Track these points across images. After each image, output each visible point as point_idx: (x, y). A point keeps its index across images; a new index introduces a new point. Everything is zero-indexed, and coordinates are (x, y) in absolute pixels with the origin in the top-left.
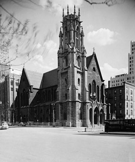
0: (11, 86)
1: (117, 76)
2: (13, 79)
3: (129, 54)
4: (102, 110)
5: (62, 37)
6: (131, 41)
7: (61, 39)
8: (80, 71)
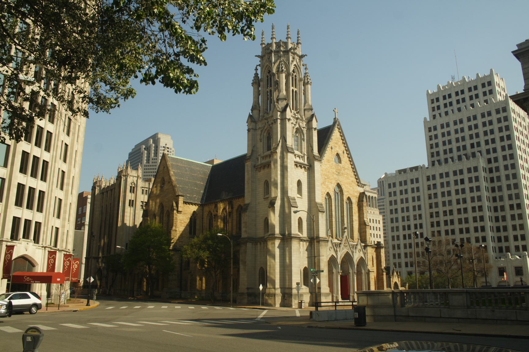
0: (130, 196)
1: (400, 172)
2: (135, 179)
3: (425, 119)
4: (362, 261)
5: (259, 86)
6: (428, 91)
7: (256, 90)
8: (301, 161)
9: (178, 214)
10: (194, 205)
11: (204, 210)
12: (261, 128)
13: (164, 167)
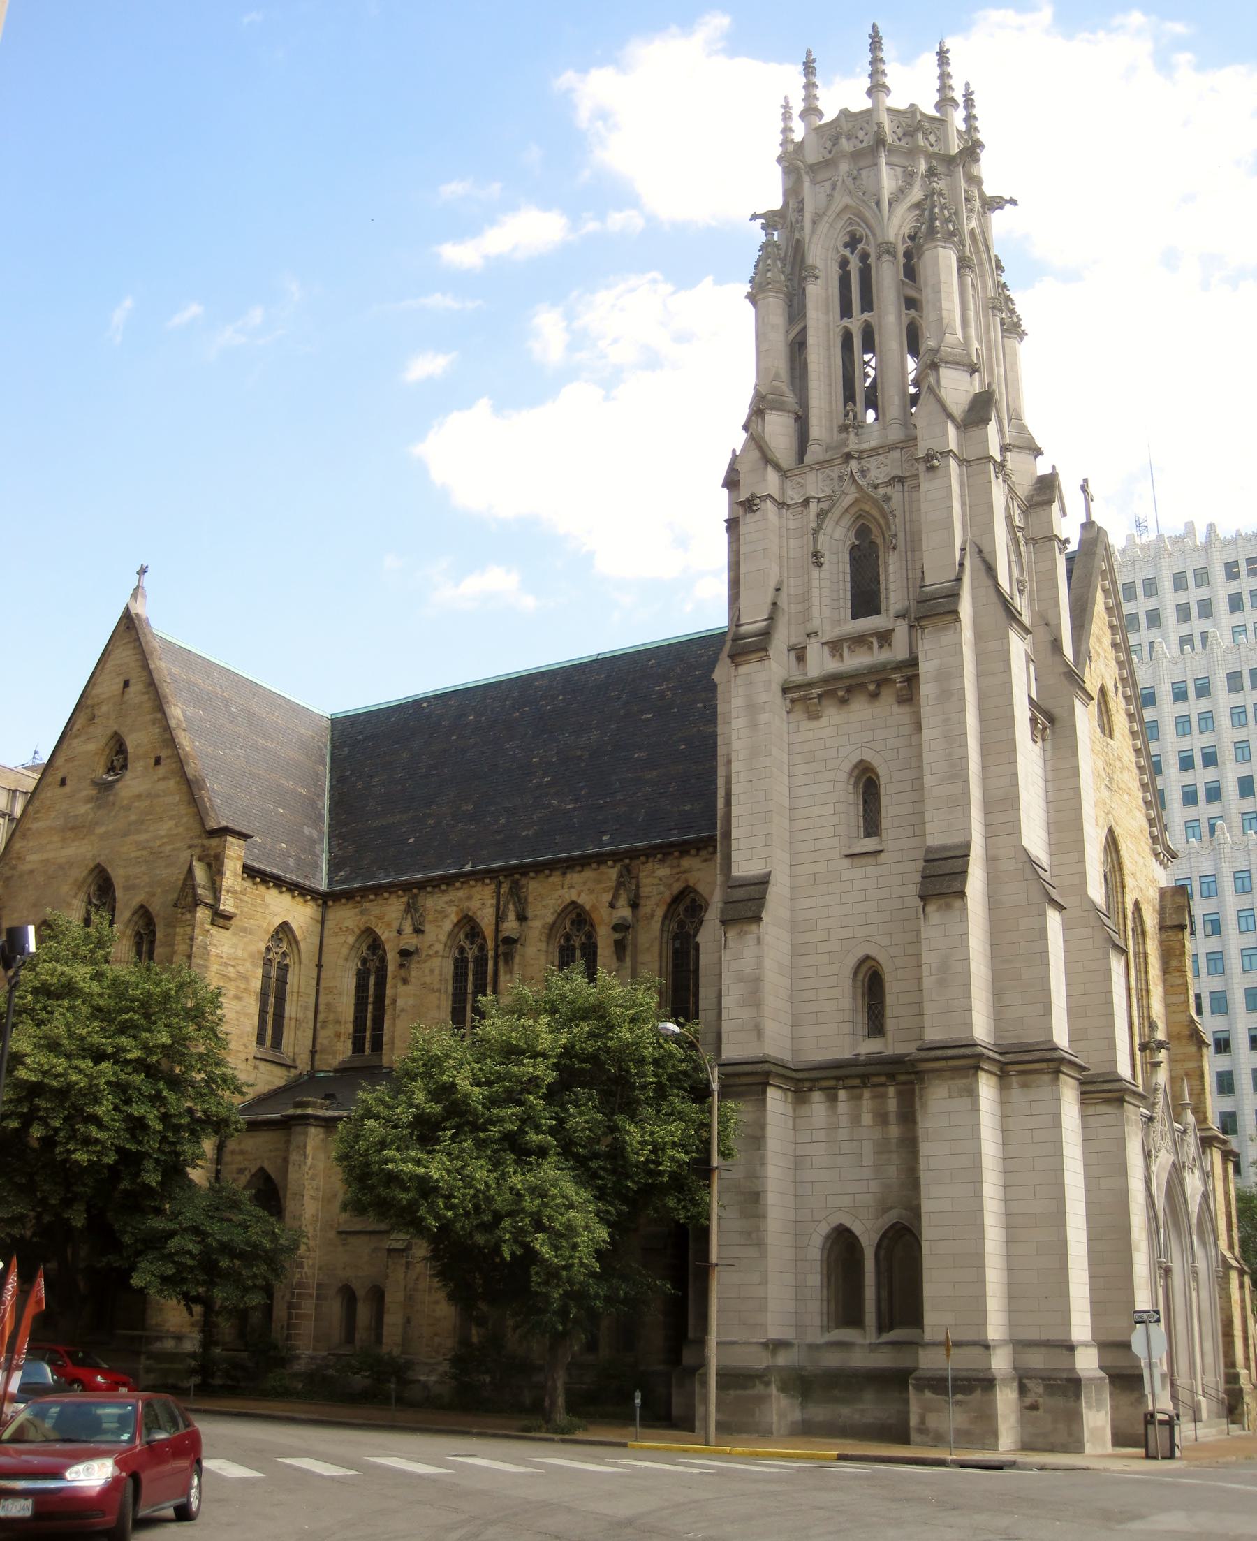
9: (214, 931)
10: (289, 890)
11: (328, 925)
12: (819, 500)
13: (126, 684)
